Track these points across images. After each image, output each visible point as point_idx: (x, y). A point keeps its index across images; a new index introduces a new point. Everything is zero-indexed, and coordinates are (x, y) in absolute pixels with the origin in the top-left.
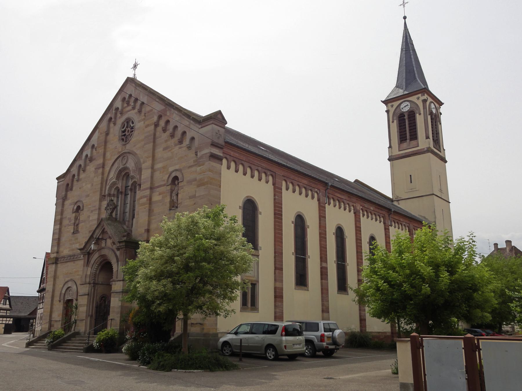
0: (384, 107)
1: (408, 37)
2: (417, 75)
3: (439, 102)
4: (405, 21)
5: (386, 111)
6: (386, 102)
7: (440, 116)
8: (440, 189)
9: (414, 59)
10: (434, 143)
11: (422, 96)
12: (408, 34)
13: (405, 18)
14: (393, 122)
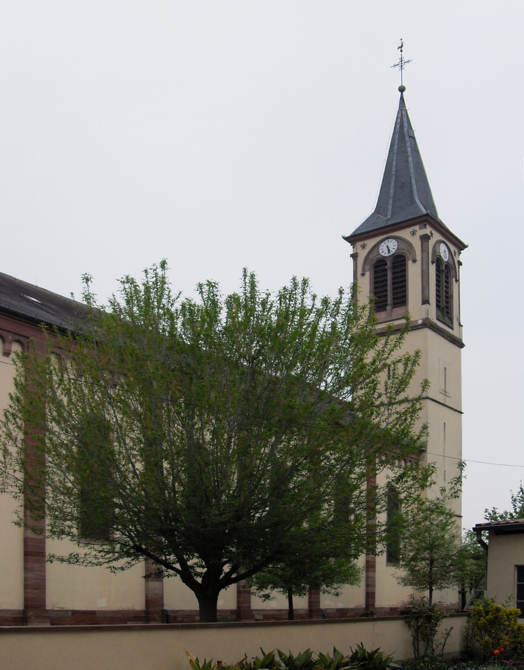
0: (349, 249)
1: (406, 124)
2: (415, 193)
3: (439, 228)
4: (402, 94)
5: (351, 255)
6: (353, 239)
7: (459, 268)
8: (444, 390)
9: (413, 164)
10: (440, 313)
11: (420, 229)
12: (405, 119)
13: (402, 89)
14: (363, 275)
